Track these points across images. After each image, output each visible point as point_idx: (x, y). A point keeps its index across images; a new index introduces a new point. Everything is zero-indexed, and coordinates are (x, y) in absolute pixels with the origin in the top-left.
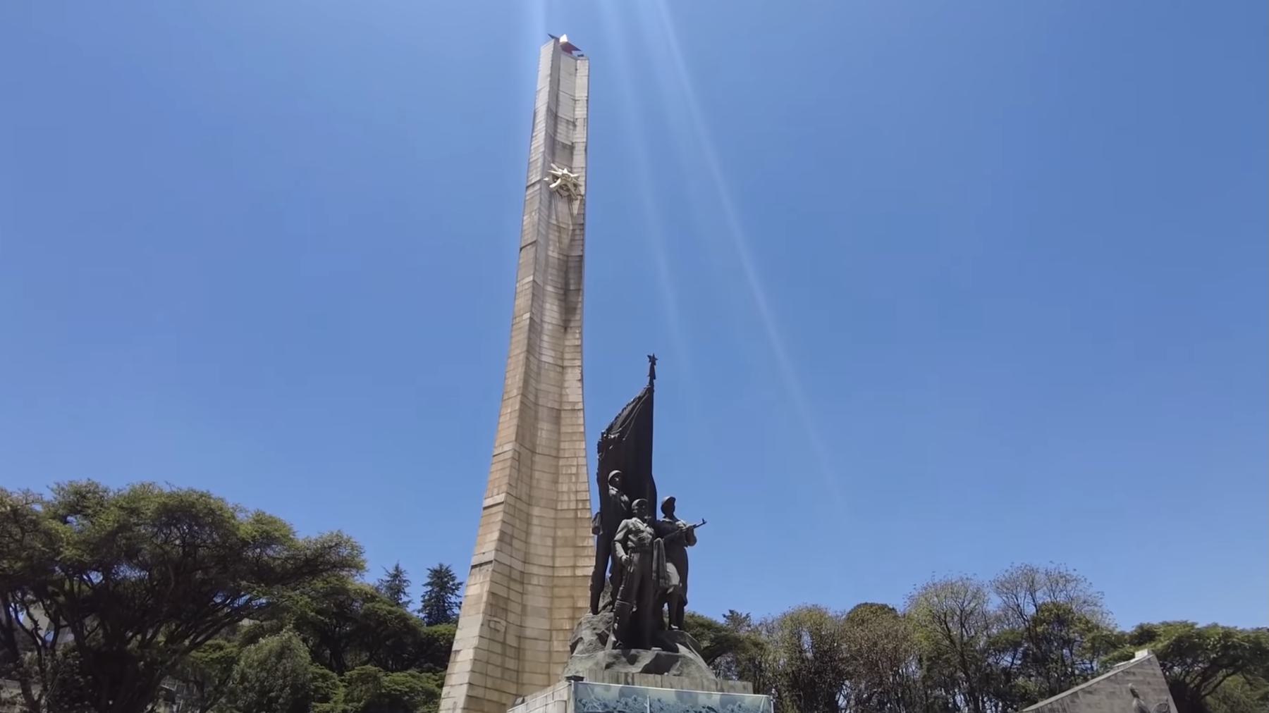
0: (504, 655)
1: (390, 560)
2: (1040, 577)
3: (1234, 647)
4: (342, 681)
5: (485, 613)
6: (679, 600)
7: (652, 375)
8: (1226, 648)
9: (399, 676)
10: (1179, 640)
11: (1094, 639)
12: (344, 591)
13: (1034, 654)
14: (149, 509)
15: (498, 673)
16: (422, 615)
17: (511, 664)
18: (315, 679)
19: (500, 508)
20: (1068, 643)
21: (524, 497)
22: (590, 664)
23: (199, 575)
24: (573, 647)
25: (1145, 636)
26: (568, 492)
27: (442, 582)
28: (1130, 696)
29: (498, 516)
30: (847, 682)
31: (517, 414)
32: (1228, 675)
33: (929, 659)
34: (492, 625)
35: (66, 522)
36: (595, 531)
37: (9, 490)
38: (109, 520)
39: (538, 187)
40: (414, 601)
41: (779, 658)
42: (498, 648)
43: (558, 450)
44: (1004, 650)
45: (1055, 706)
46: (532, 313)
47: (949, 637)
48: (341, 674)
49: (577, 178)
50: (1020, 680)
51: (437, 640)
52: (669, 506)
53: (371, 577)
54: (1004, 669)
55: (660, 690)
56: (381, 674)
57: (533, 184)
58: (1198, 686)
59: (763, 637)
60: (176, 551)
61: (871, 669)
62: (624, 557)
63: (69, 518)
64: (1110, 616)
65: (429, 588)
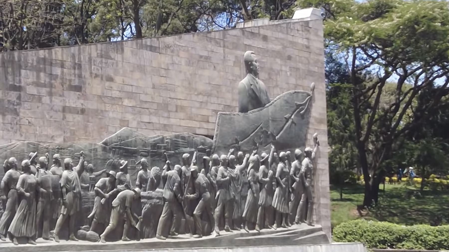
28: (241, 69)
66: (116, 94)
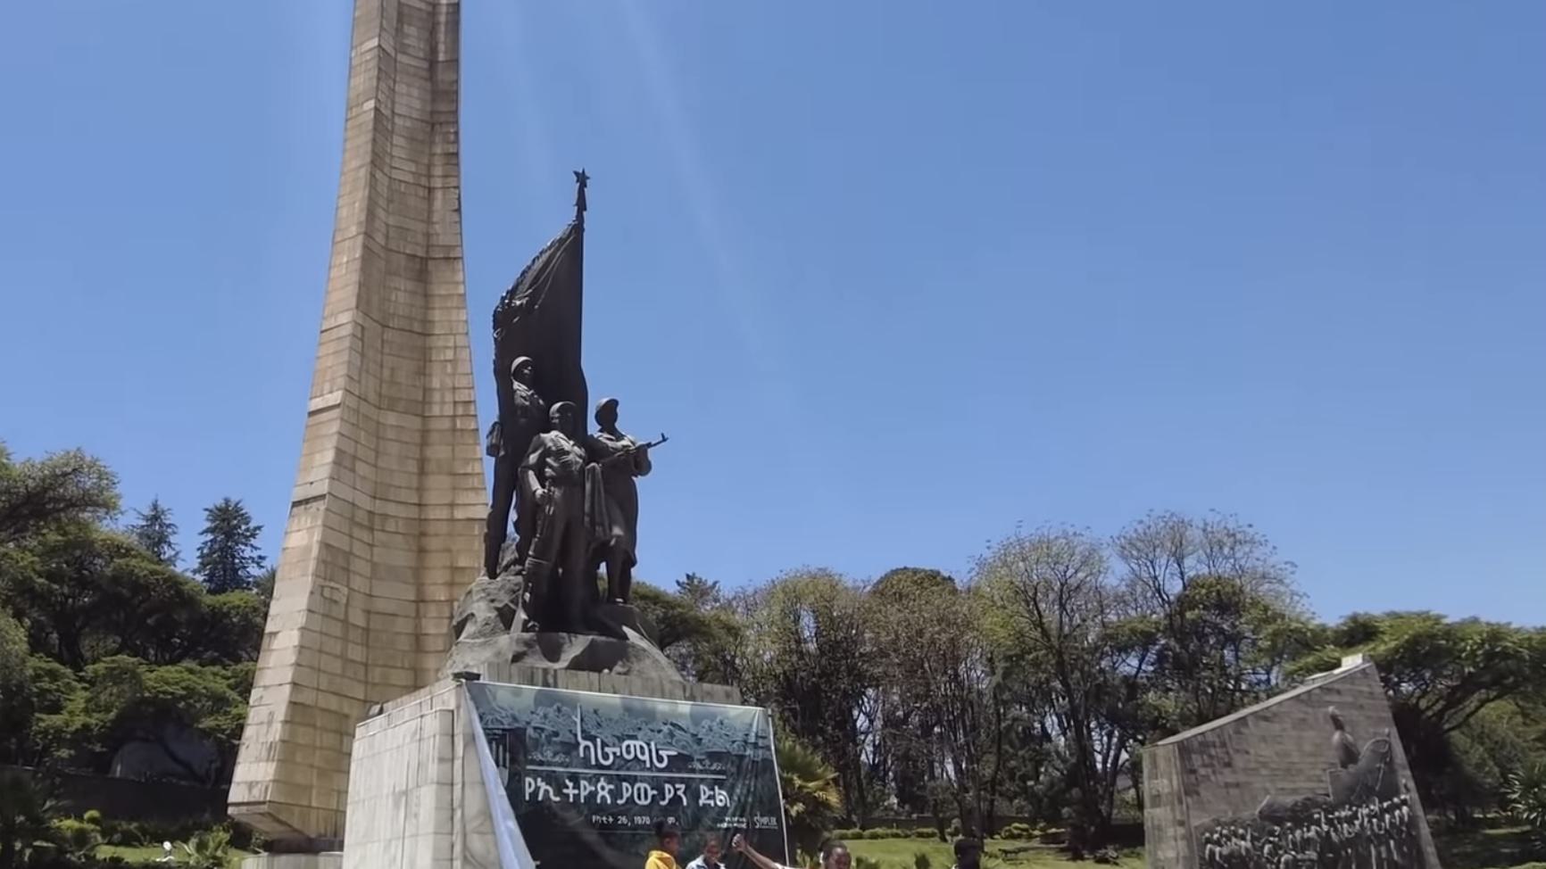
1: (158, 489)
2: (1194, 534)
3: (1505, 655)
4: (81, 680)
5: (316, 575)
7: (581, 205)
8: (1490, 656)
10: (1415, 641)
11: (1275, 634)
12: (87, 545)
13: (1176, 656)
15: (336, 666)
17: (356, 653)
18: (37, 678)
19: (335, 413)
20: (1234, 639)
21: (372, 397)
22: (487, 654)
24: (459, 629)
25: (1359, 633)
26: (442, 389)
27: (229, 525)
28: (1330, 726)
29: (332, 426)
30: (870, 692)
31: (357, 265)
32: (1489, 700)
33: (1008, 658)
34: (327, 593)
36: (492, 450)
40: (186, 555)
41: (761, 649)
42: (337, 630)
43: (426, 322)
44: (1124, 649)
45: (1210, 738)
46: (378, 100)
47: (1039, 624)
48: (77, 668)
50: (1151, 697)
51: (227, 615)
52: (608, 415)
53: (120, 525)
54: (1126, 678)
55: (596, 695)
56: (143, 668)
58: (1441, 712)
59: (739, 618)
61: (911, 673)
62: (540, 491)
64: (1304, 600)
65: (210, 537)
66: (1253, 765)
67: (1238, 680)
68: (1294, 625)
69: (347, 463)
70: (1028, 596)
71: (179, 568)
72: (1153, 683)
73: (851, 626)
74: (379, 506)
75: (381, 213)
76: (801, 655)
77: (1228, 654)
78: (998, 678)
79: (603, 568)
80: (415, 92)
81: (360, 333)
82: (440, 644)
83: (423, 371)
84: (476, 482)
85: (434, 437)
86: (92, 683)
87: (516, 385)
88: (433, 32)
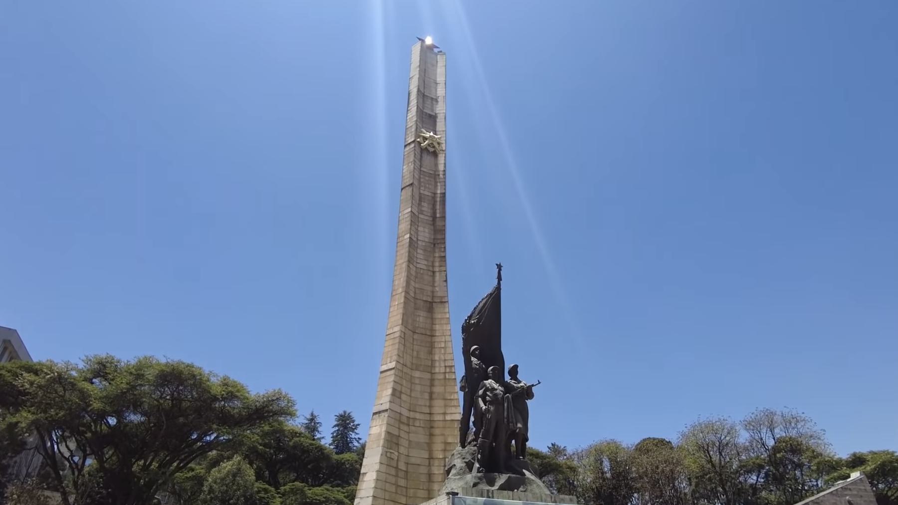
0: (397, 476)
1: (314, 408)
2: (778, 418)
4: (278, 493)
5: (383, 446)
6: (523, 438)
7: (499, 278)
9: (318, 490)
10: (883, 464)
11: (819, 463)
12: (282, 431)
13: (774, 474)
14: (150, 374)
15: (393, 489)
16: (332, 447)
17: (402, 482)
18: (259, 492)
19: (392, 372)
20: (800, 466)
21: (409, 364)
22: (461, 483)
23: (181, 420)
24: (448, 472)
25: (857, 461)
26: (440, 360)
27: (345, 423)
29: (391, 378)
30: (636, 495)
31: (402, 306)
35: (92, 383)
36: (462, 389)
37: (56, 361)
38: (122, 383)
39: (413, 145)
40: (326, 437)
41: (586, 477)
42: (393, 472)
43: (432, 330)
44: (750, 472)
48: (277, 488)
49: (440, 138)
50: (764, 494)
52: (514, 371)
53: (297, 423)
54: (751, 485)
56: (306, 488)
57: (409, 144)
59: (575, 463)
60: (167, 404)
61: (654, 486)
62: (484, 407)
63: (94, 380)
67: (803, 485)
68: (827, 459)
69: (398, 394)
70: (704, 449)
71: (323, 442)
72: (765, 487)
73: (626, 465)
74: (412, 415)
75: (412, 283)
76: (604, 480)
77: (798, 473)
78: (693, 487)
79: (513, 442)
80: (427, 230)
81: (403, 337)
82: (440, 478)
83: (431, 352)
84: (455, 403)
85: (436, 383)
86: (284, 495)
87: (473, 359)
88: (434, 205)
